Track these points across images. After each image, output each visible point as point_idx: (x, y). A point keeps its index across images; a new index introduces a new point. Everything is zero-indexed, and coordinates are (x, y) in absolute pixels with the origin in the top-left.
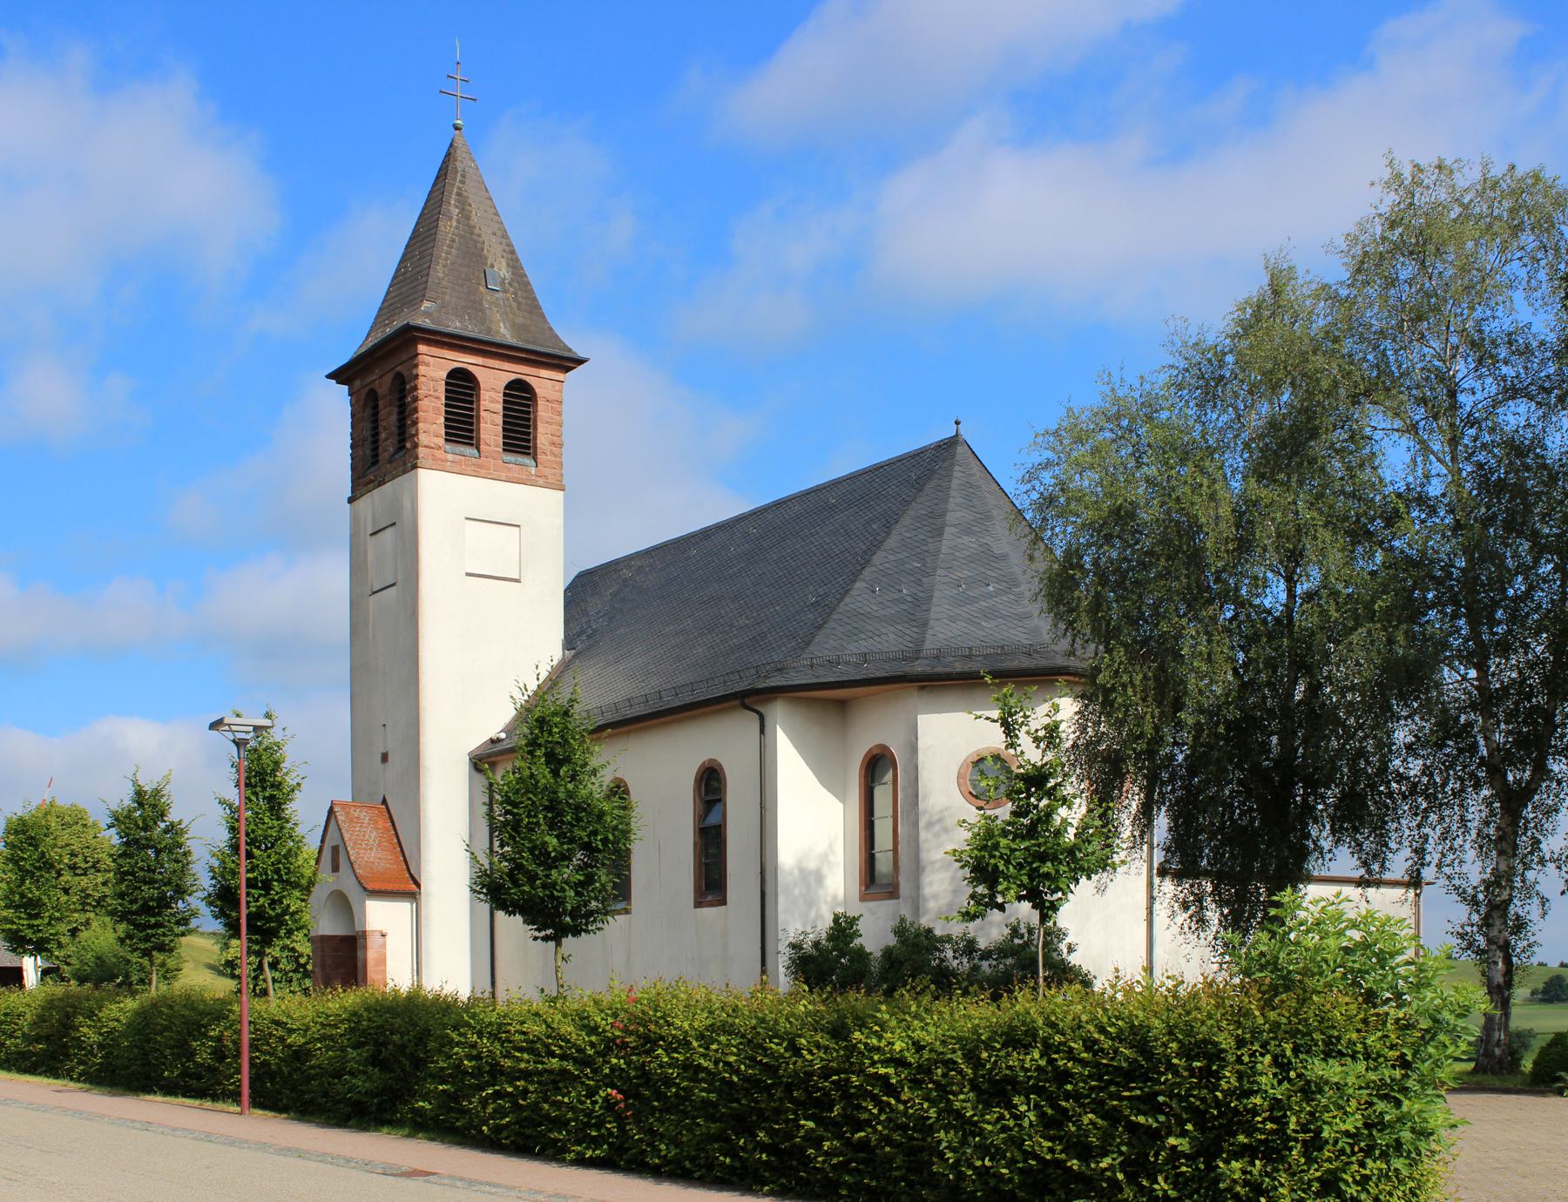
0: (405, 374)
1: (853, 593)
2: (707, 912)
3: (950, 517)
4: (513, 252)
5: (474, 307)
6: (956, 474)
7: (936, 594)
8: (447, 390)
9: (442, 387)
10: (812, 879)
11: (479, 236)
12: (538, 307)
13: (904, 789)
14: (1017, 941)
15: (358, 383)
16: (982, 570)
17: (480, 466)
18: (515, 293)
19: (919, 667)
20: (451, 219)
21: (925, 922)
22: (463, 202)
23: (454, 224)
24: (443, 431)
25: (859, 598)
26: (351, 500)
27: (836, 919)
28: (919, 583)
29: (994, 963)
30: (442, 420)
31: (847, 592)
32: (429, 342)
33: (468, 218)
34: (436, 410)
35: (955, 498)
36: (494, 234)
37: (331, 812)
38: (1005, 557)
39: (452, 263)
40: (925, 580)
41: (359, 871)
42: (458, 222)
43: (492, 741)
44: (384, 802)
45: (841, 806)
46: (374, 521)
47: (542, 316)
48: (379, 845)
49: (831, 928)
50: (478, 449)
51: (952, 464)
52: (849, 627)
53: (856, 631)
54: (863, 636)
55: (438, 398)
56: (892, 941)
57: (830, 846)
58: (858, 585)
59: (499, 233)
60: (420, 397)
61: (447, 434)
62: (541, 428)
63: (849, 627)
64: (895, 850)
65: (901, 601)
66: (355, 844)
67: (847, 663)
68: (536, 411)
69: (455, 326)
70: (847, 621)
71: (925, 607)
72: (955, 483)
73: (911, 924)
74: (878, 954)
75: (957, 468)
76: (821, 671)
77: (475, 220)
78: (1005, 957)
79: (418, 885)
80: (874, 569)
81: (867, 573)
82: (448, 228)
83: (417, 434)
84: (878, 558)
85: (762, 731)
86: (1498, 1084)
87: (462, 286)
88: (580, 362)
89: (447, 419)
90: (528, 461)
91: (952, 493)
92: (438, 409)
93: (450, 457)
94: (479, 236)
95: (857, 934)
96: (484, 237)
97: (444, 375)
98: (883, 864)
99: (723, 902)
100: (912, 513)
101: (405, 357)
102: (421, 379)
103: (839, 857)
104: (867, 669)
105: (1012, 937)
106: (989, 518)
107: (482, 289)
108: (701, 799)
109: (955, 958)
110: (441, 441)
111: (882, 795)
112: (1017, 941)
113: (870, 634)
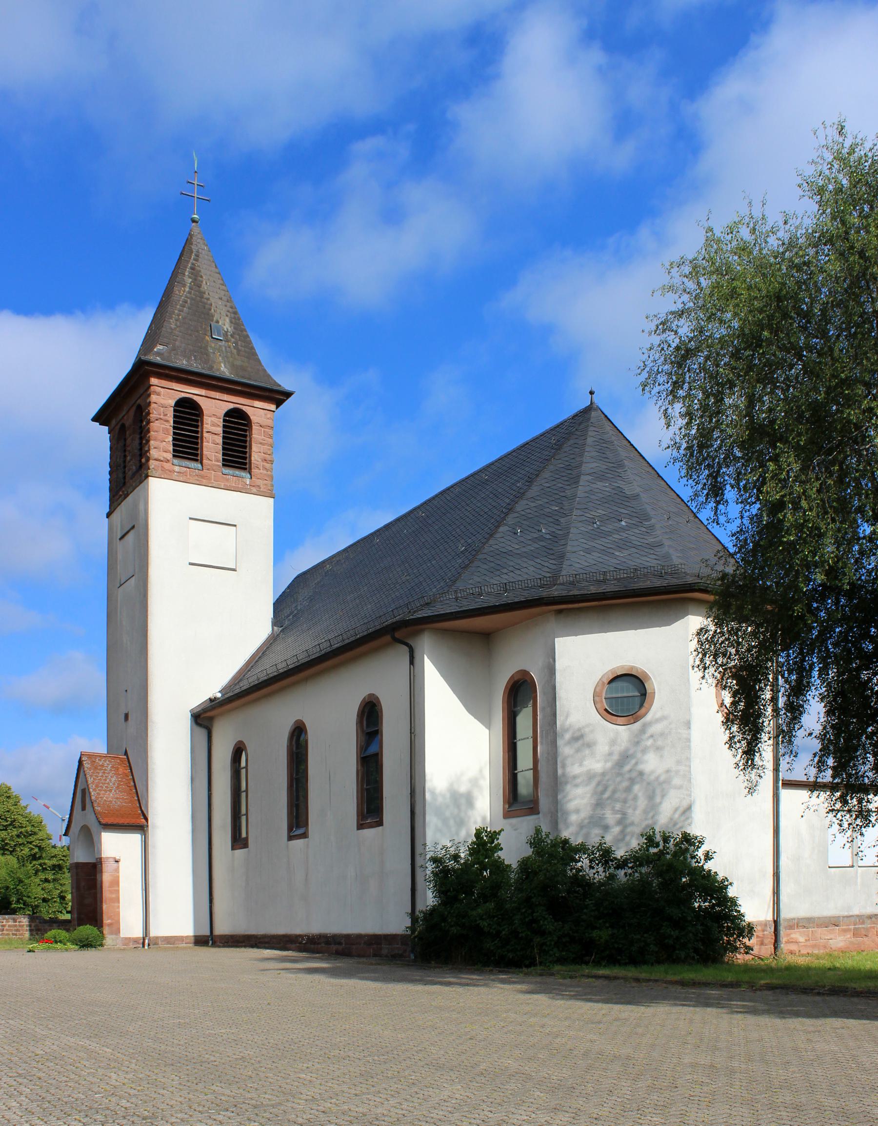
0: (142, 404)
1: (497, 535)
2: (368, 833)
3: (586, 468)
4: (235, 313)
5: (202, 352)
6: (590, 433)
7: (572, 530)
8: (175, 416)
9: (171, 413)
10: (463, 801)
11: (208, 299)
12: (255, 354)
13: (543, 709)
14: (653, 850)
15: (114, 422)
16: (615, 508)
17: (203, 477)
18: (236, 343)
19: (556, 592)
20: (184, 286)
21: (565, 834)
22: (196, 274)
23: (187, 289)
24: (171, 448)
25: (502, 540)
26: (108, 515)
27: (478, 834)
28: (557, 522)
29: (630, 871)
30: (170, 438)
31: (491, 536)
32: (160, 376)
33: (200, 286)
34: (166, 431)
35: (590, 453)
36: (221, 299)
37: (80, 762)
38: (636, 497)
39: (184, 318)
40: (562, 520)
41: (97, 808)
42: (191, 288)
43: (211, 700)
44: (126, 753)
45: (487, 731)
46: (122, 528)
47: (259, 361)
48: (118, 787)
49: (473, 843)
50: (202, 463)
51: (588, 426)
52: (492, 565)
53: (499, 567)
54: (505, 571)
55: (167, 421)
56: (529, 852)
57: (481, 771)
58: (501, 529)
59: (225, 298)
60: (152, 420)
61: (174, 451)
62: (255, 448)
63: (492, 565)
64: (535, 769)
65: (542, 539)
66: (97, 786)
67: (489, 594)
68: (251, 435)
69: (182, 363)
70: (492, 559)
71: (563, 542)
72: (590, 440)
73: (547, 836)
74: (515, 866)
75: (592, 428)
76: (465, 602)
77: (204, 287)
78: (641, 865)
79: (146, 819)
80: (516, 515)
81: (511, 519)
82: (182, 293)
83: (149, 450)
84: (520, 506)
85: (412, 662)
86: (822, 934)
87: (191, 335)
88: (288, 395)
89: (174, 439)
90: (243, 474)
91: (587, 449)
92: (167, 430)
93: (177, 469)
94: (208, 299)
95: (498, 848)
96: (212, 300)
97: (173, 403)
98: (525, 779)
99: (380, 823)
100: (551, 467)
101: (141, 391)
102: (153, 405)
103: (485, 783)
104: (507, 597)
105: (648, 847)
106: (621, 465)
107: (208, 338)
108: (363, 731)
109: (591, 867)
110: (169, 456)
111: (524, 721)
112: (653, 850)
113: (511, 569)
